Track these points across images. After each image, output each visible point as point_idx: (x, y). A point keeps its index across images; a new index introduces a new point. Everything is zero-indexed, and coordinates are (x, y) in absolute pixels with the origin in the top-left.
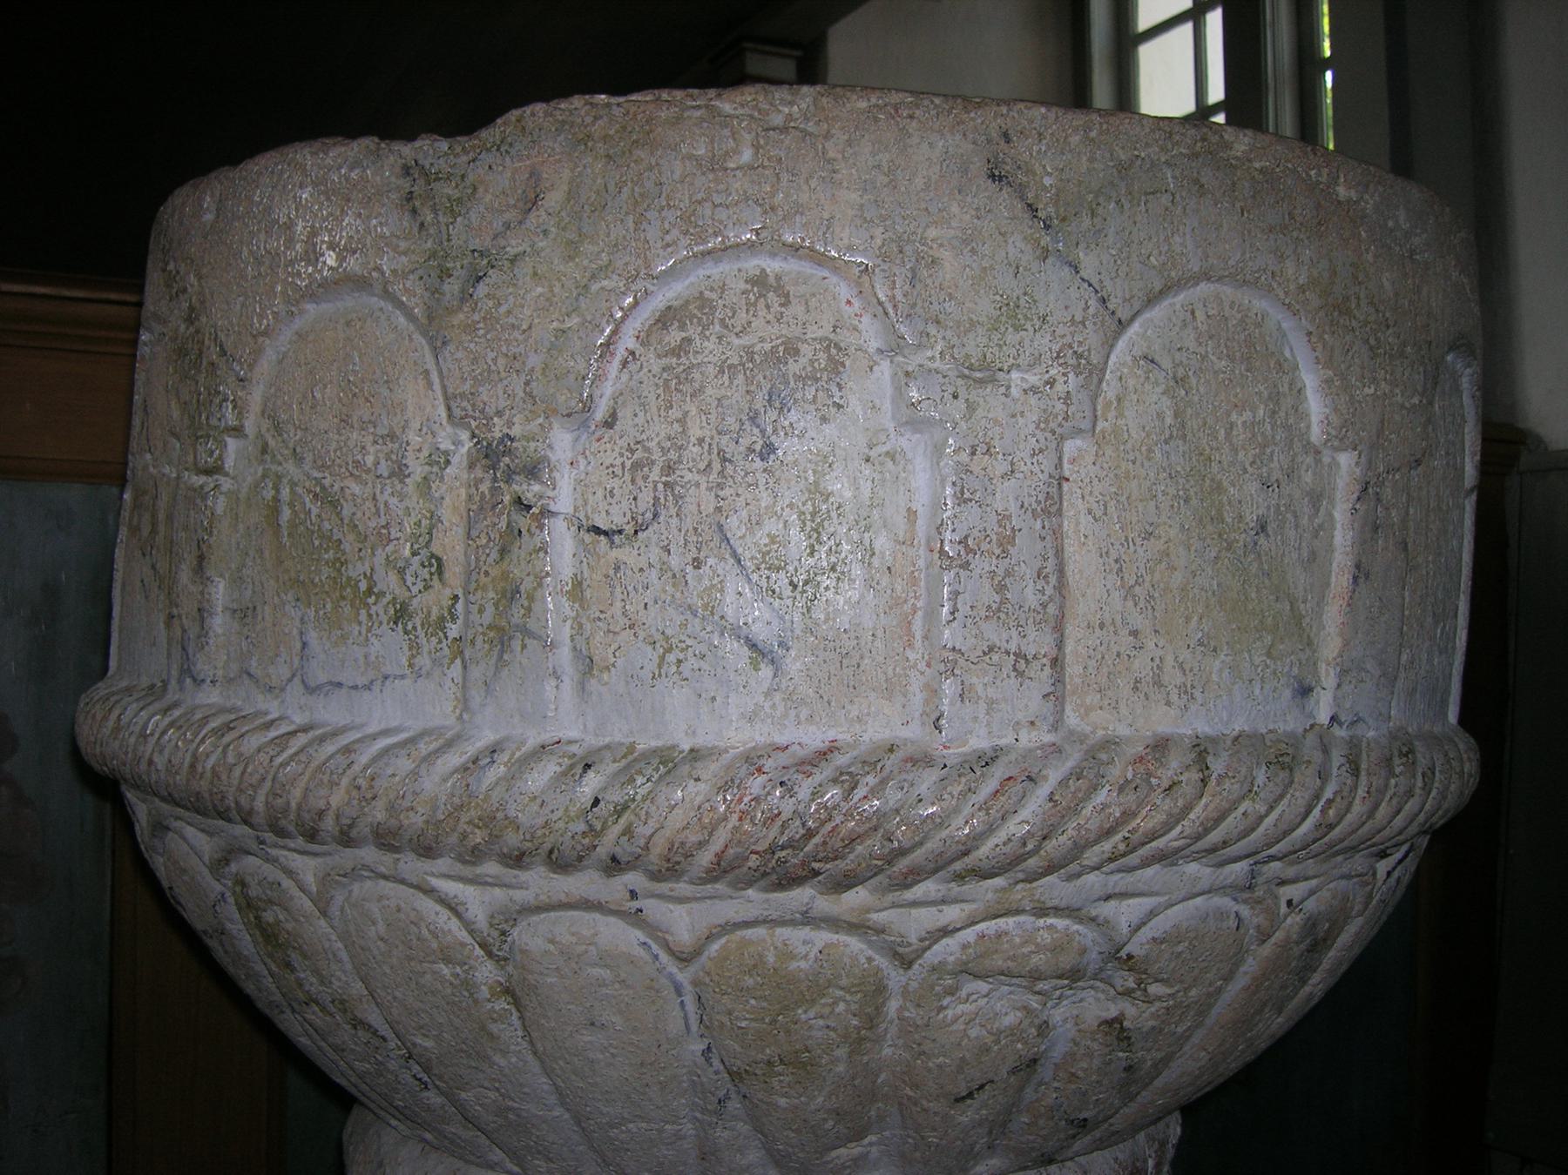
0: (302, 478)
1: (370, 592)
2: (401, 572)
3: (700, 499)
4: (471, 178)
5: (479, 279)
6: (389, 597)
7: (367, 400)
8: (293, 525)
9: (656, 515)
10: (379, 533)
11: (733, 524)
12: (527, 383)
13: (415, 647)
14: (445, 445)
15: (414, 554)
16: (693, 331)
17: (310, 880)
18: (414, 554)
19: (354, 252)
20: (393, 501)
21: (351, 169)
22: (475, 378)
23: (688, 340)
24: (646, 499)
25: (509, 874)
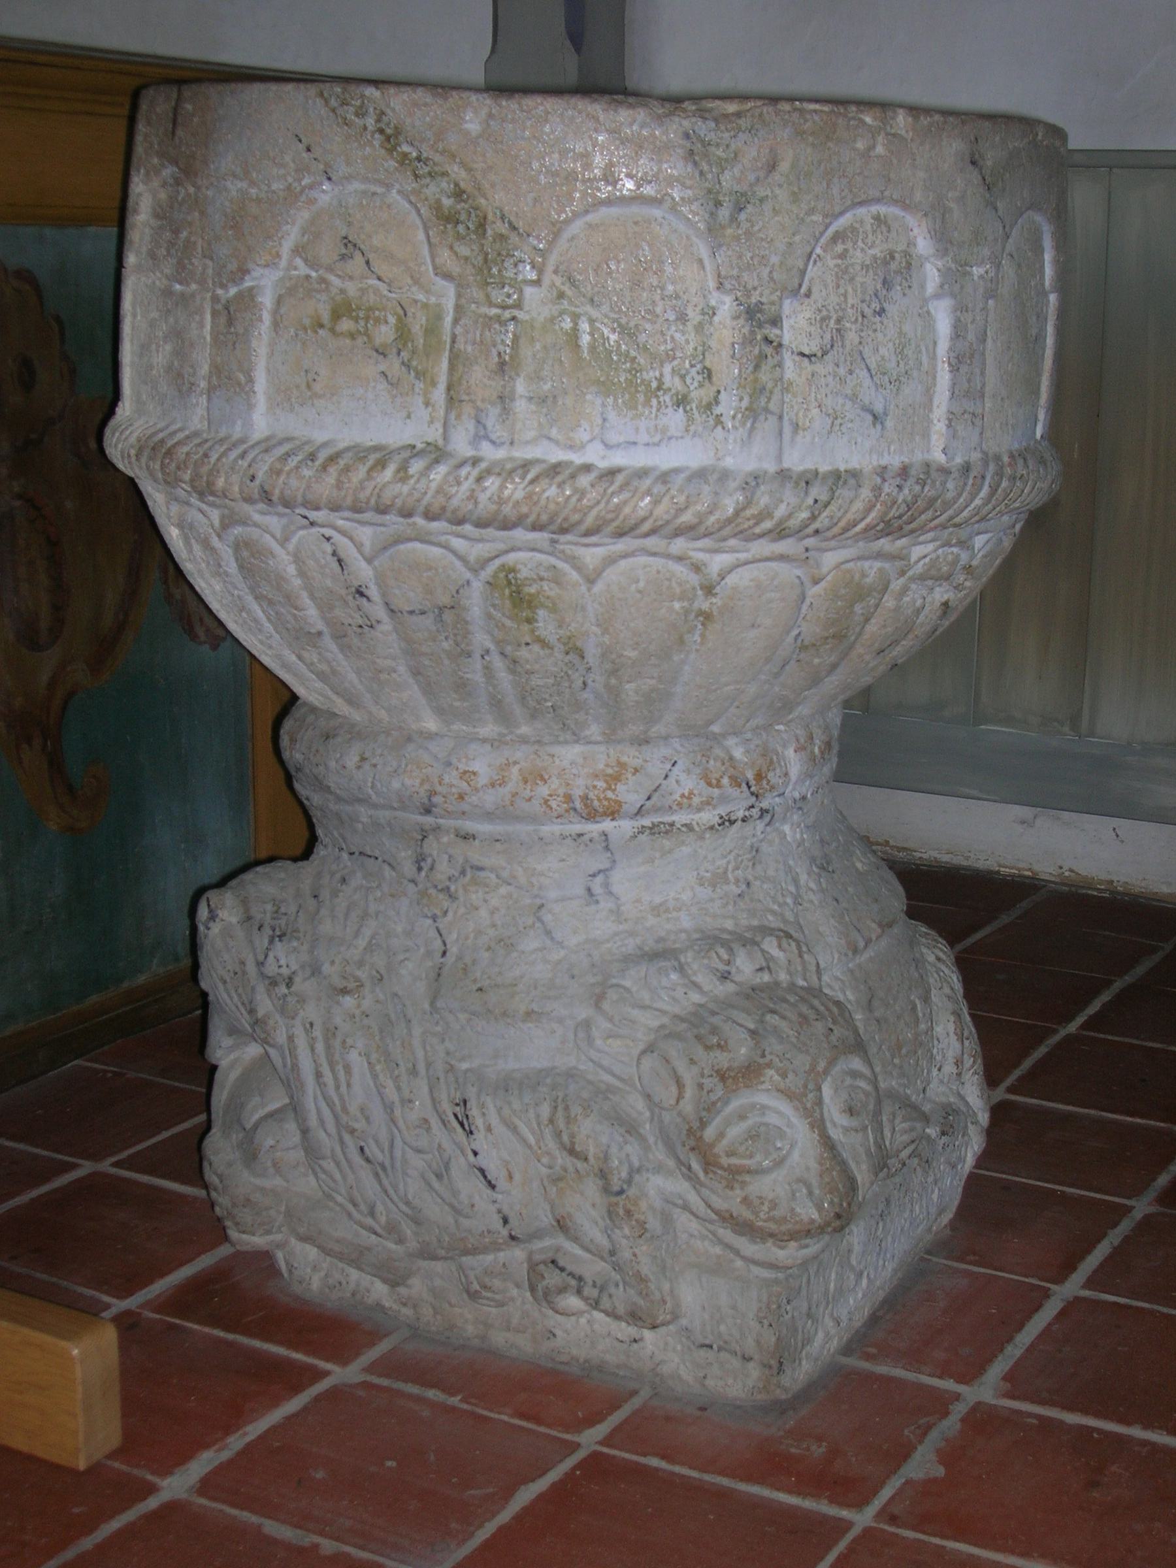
0: (600, 316)
1: (659, 388)
2: (683, 377)
3: (852, 337)
4: (733, 146)
5: (741, 209)
6: (673, 391)
7: (656, 273)
8: (592, 348)
9: (832, 346)
10: (667, 354)
11: (867, 352)
12: (771, 272)
13: (690, 420)
14: (713, 303)
15: (692, 366)
16: (849, 245)
17: (368, 544)
18: (692, 366)
19: (650, 182)
20: (678, 336)
21: (642, 127)
22: (739, 268)
23: (846, 250)
24: (828, 337)
25: (379, 518)
